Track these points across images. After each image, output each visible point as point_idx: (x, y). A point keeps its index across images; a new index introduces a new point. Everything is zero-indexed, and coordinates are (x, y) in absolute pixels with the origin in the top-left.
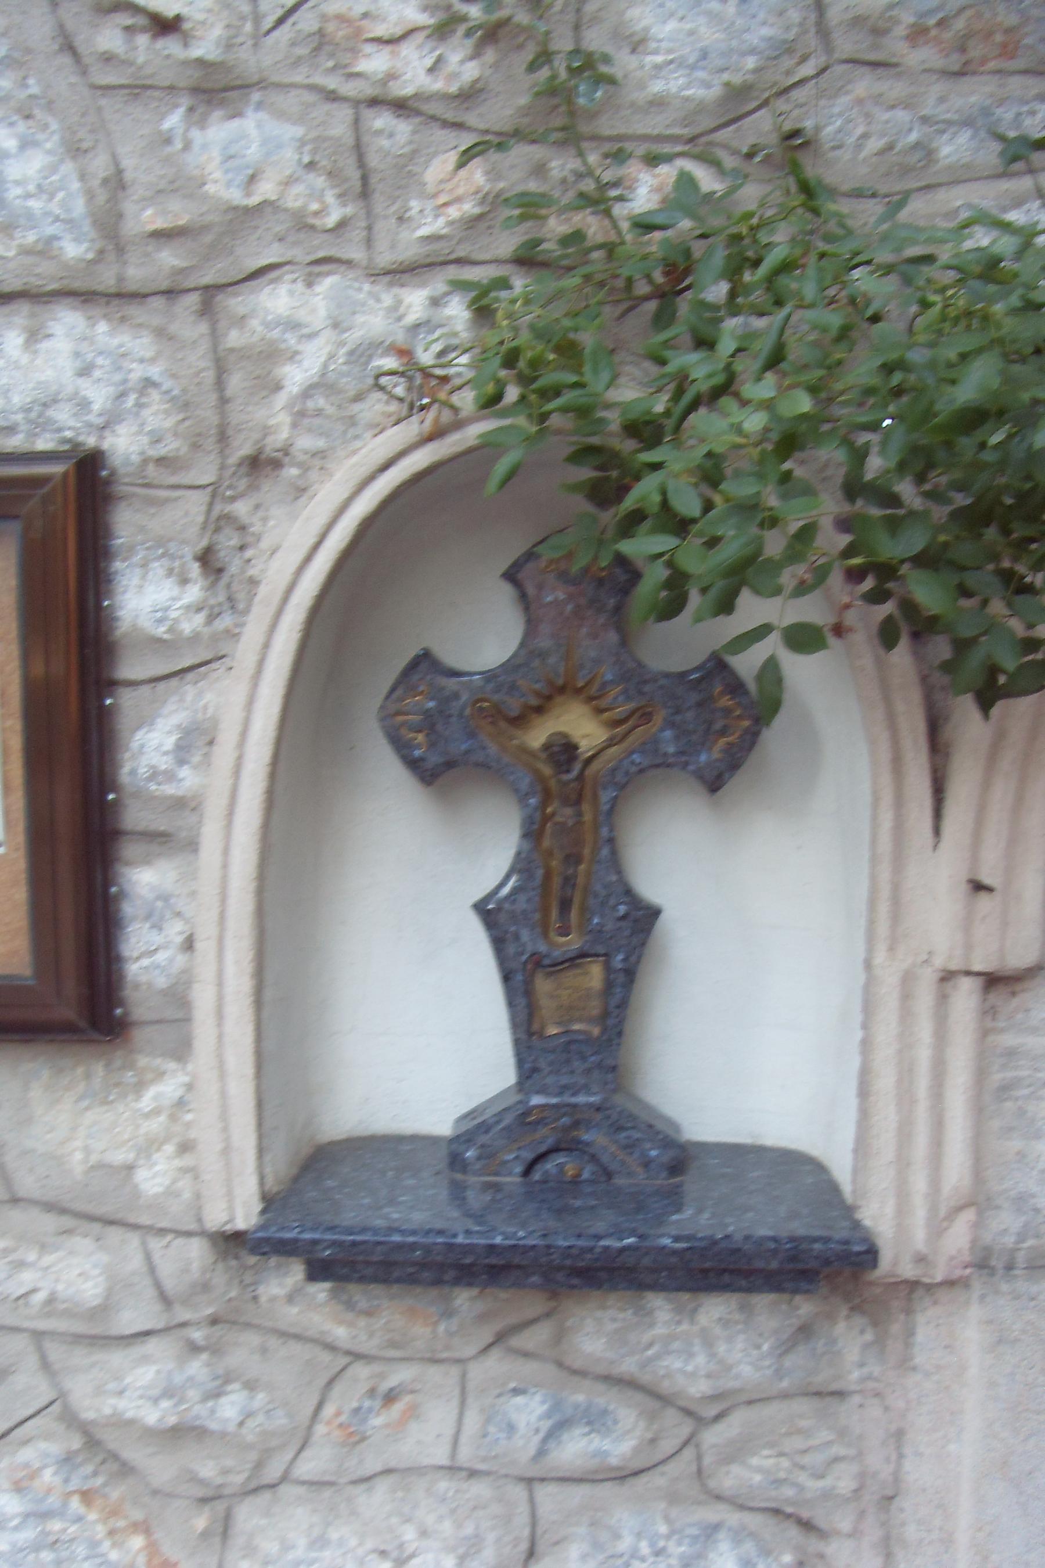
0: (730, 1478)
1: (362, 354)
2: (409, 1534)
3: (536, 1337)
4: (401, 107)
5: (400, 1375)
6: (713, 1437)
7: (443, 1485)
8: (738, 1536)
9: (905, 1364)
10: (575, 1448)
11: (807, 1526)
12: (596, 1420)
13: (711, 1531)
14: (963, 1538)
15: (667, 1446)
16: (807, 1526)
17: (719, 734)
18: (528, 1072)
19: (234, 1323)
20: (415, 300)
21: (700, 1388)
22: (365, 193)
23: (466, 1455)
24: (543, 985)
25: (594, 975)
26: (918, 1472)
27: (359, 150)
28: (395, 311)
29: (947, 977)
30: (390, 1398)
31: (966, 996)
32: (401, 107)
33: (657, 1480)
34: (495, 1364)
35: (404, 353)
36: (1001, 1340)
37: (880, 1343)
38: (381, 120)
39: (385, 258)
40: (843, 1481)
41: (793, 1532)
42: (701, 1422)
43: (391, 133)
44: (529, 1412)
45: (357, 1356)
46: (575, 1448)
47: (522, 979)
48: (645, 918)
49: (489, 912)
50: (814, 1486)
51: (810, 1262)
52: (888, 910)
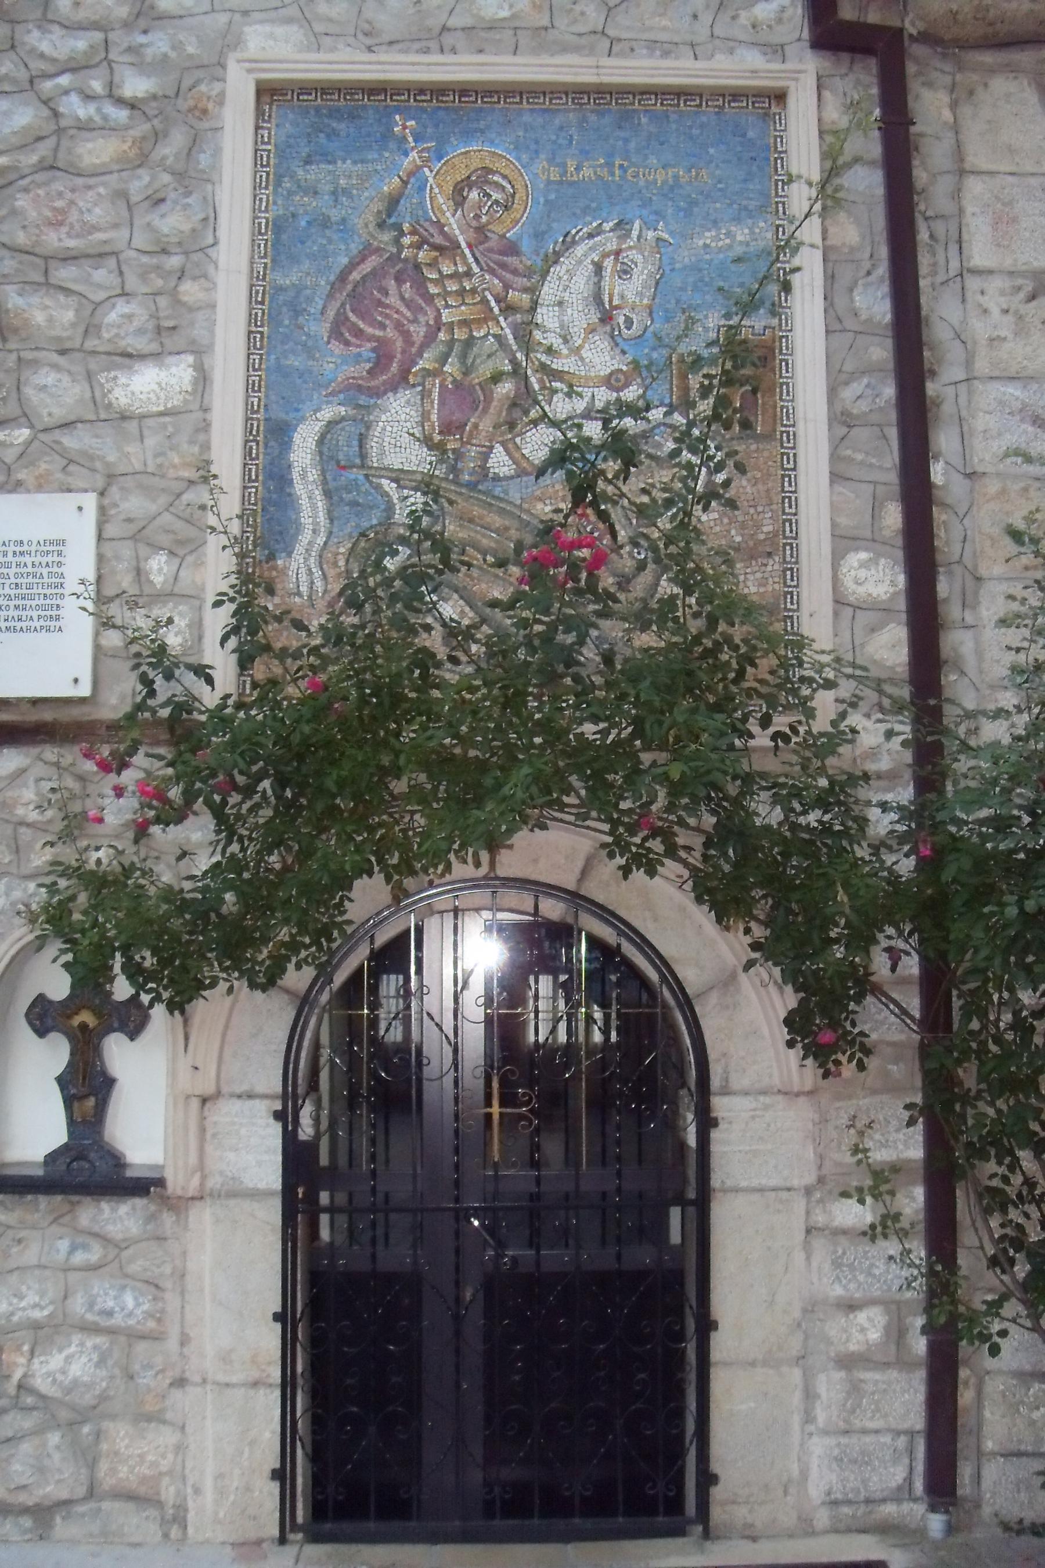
0: (134, 1268)
1: (13, 904)
2: (24, 1288)
3: (67, 1219)
4: (28, 825)
5: (22, 1234)
6: (125, 1254)
7: (37, 1272)
8: (134, 1289)
9: (186, 1228)
10: (79, 1258)
11: (157, 1286)
12: (85, 1247)
13: (123, 1288)
14: (207, 1290)
15: (111, 1257)
16: (157, 1286)
17: (131, 1021)
18: (70, 1133)
19: (243, 1544)
20: (32, 886)
21: (120, 1236)
22: (17, 851)
23: (43, 1261)
24: (76, 1105)
25: (91, 1102)
26: (191, 1266)
27: (16, 839)
28: (25, 890)
29: (188, 1097)
30: (20, 1241)
31: (195, 1103)
32: (28, 825)
33: (107, 1269)
34: (54, 1228)
35: (26, 905)
36: (217, 1221)
37: (178, 1221)
38: (23, 830)
39: (25, 871)
40: (167, 1269)
41: (153, 1289)
42: (122, 1249)
43: (25, 834)
44: (64, 1245)
45: (9, 1227)
46: (79, 1258)
47: (69, 1102)
48: (109, 1082)
49: (59, 1080)
50: (157, 1271)
51: (144, 1187)
52: (173, 1074)
